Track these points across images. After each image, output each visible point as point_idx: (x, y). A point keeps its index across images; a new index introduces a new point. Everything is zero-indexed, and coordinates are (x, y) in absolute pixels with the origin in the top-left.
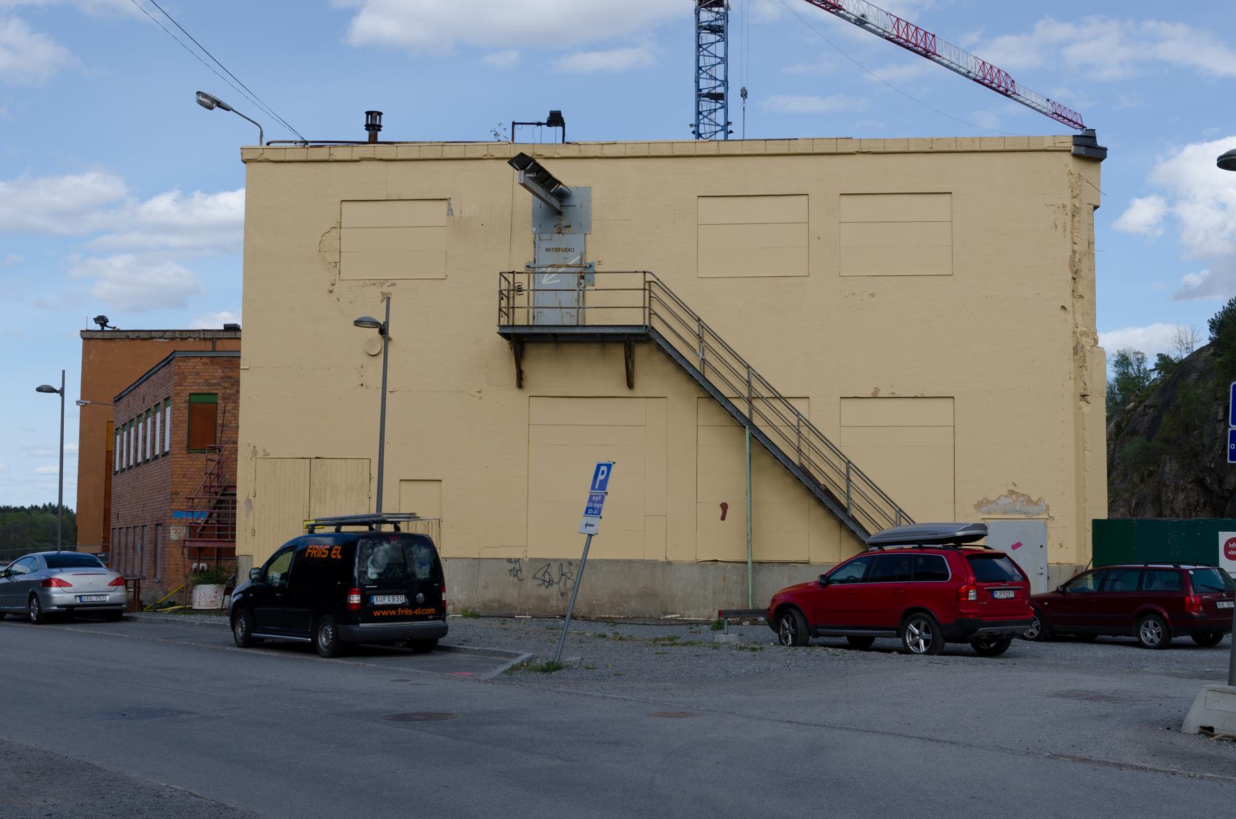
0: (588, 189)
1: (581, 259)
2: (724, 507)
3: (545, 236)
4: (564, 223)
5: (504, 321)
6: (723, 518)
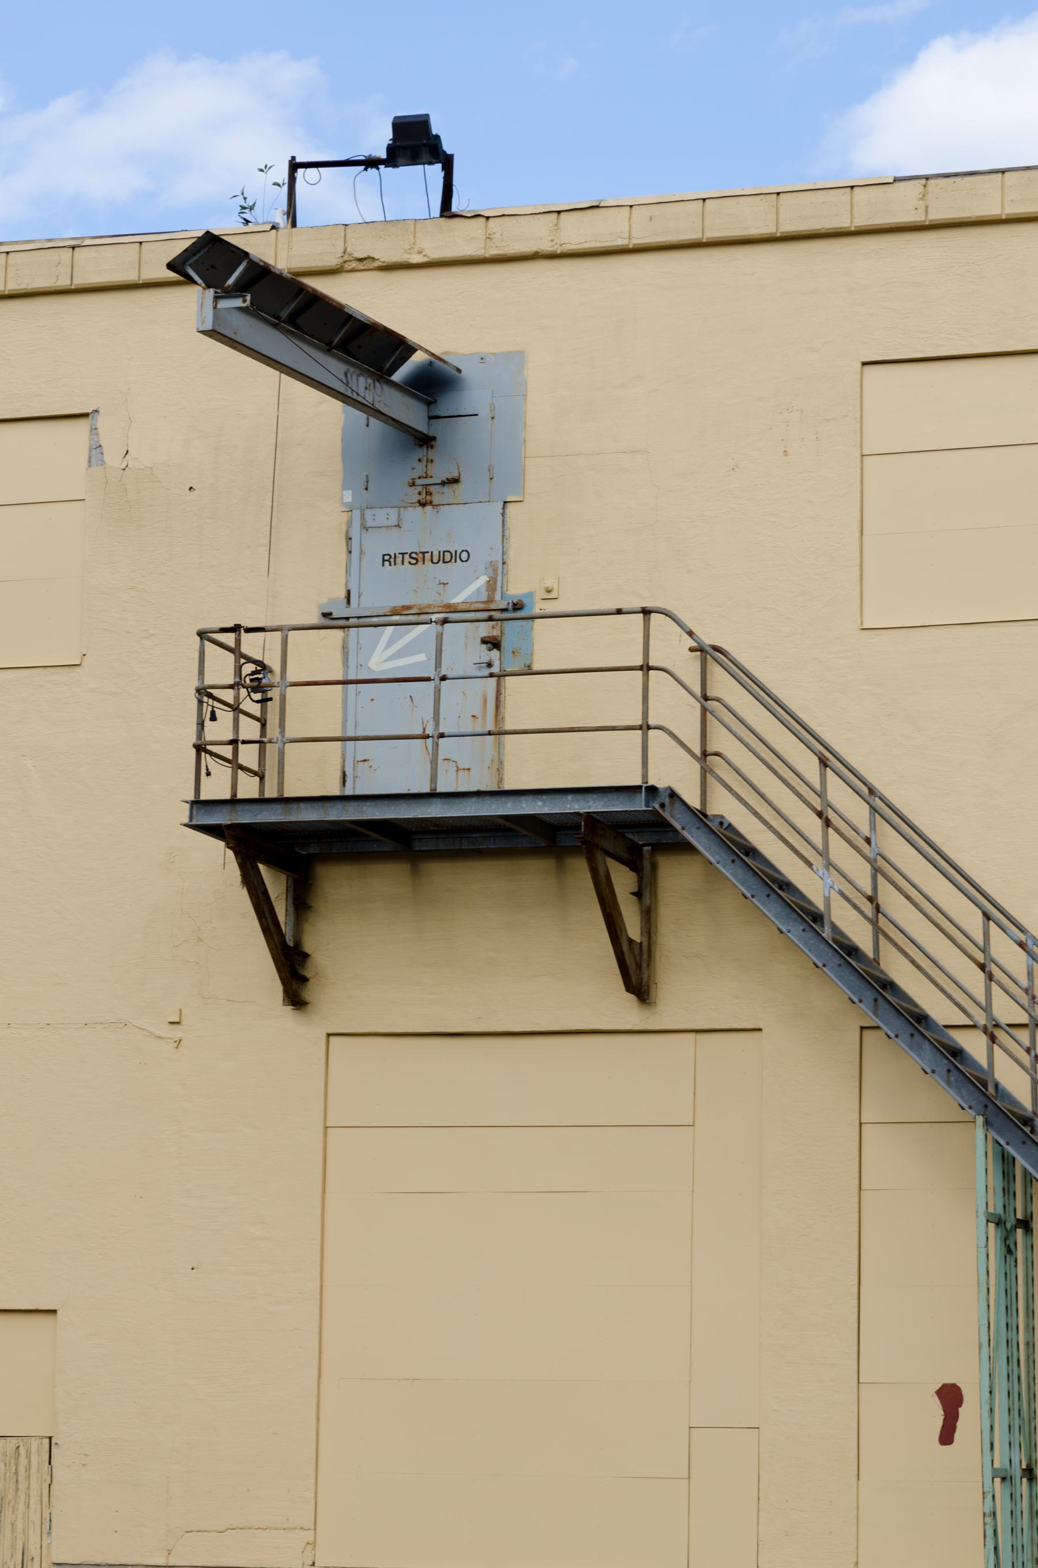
0: (516, 359)
1: (491, 585)
2: (950, 1398)
3: (381, 517)
4: (439, 473)
5: (217, 785)
6: (947, 1437)
